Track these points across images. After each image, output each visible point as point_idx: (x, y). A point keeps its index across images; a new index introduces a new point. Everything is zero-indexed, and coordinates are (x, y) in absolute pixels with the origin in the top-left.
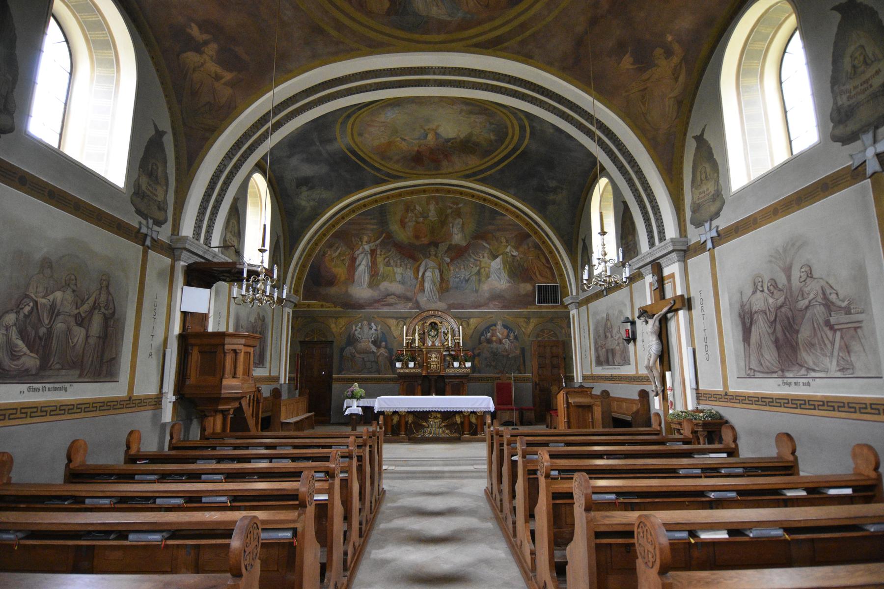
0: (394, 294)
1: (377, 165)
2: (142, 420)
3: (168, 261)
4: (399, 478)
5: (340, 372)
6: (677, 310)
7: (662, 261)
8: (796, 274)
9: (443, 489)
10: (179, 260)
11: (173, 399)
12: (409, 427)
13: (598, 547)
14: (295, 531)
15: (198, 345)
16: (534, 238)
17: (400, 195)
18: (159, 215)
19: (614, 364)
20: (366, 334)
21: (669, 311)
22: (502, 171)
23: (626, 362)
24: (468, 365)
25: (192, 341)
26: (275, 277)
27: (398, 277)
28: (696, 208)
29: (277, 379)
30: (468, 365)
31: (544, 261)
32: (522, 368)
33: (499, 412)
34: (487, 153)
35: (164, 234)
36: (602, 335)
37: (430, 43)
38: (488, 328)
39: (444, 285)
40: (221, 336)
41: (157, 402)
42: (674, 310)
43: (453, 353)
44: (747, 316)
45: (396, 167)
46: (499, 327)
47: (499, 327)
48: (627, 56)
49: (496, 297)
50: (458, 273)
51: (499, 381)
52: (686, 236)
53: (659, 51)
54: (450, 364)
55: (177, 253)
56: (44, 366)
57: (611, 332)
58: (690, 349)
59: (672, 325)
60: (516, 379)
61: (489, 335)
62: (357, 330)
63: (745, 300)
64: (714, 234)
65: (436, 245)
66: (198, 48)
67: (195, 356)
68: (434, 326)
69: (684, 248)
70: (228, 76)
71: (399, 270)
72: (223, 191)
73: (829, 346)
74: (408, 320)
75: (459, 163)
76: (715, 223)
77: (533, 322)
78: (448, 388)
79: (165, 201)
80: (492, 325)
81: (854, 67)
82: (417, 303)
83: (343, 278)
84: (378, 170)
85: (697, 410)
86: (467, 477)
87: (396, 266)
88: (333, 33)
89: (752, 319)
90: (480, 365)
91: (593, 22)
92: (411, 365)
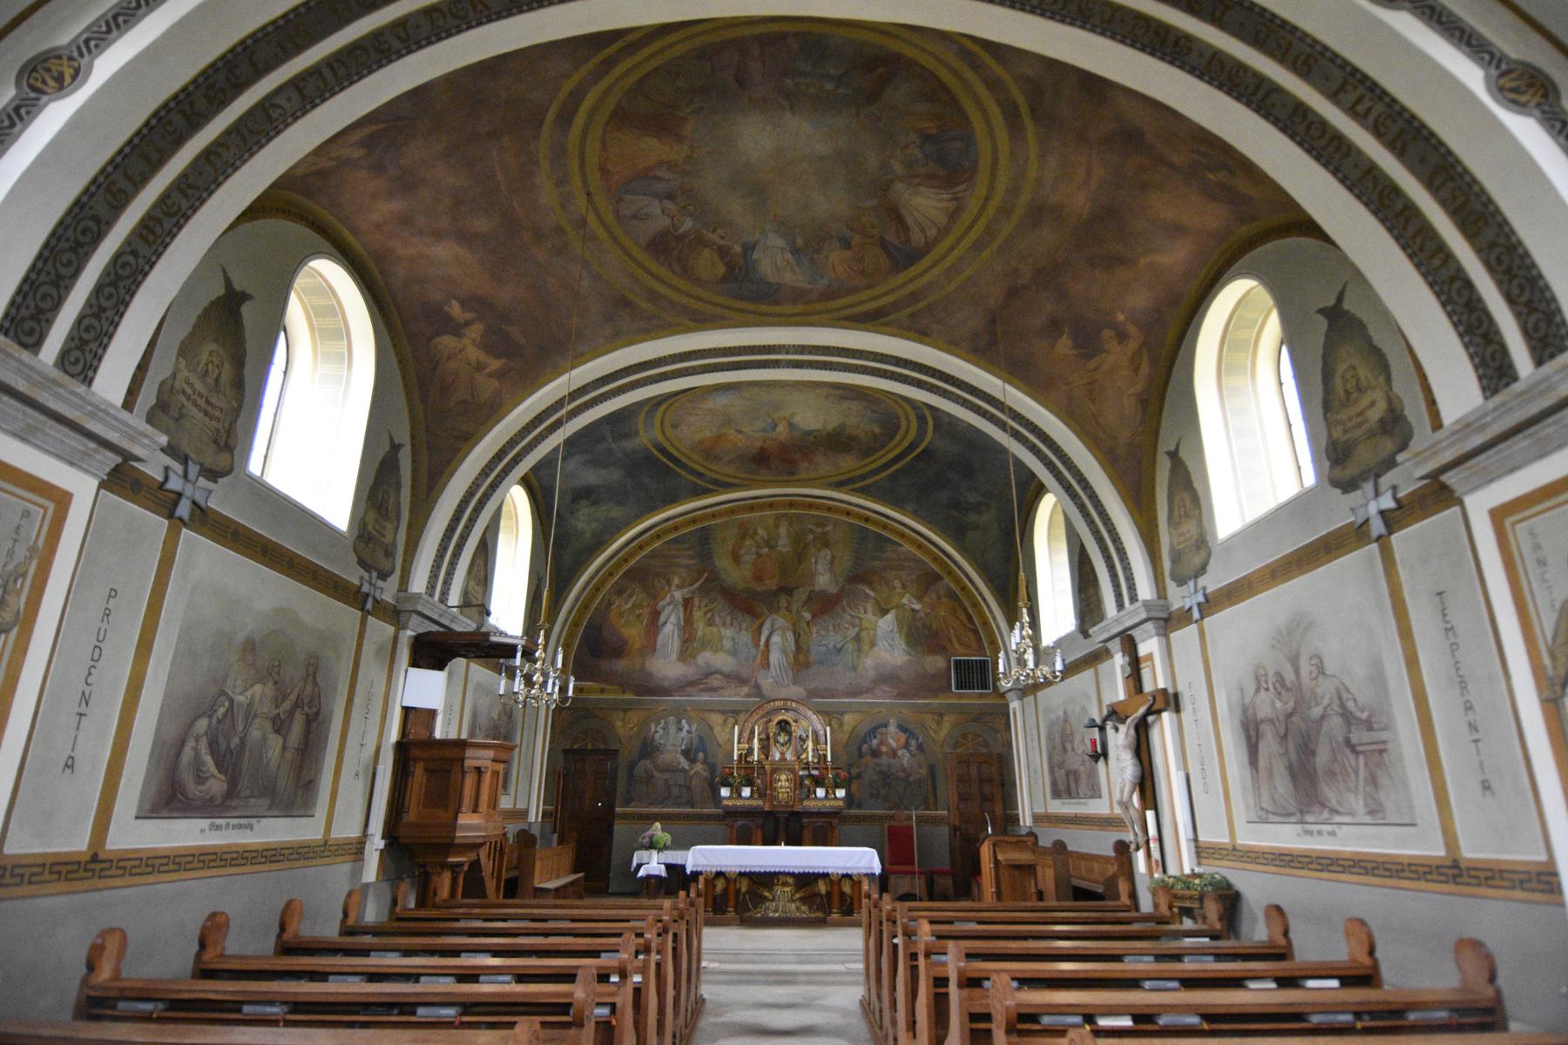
0: (718, 672)
1: (697, 468)
2: (337, 877)
3: (390, 629)
4: (726, 983)
5: (627, 803)
6: (1159, 712)
7: (1135, 633)
8: (1305, 668)
9: (792, 1000)
10: (405, 627)
11: (381, 844)
12: (742, 900)
13: (972, 1030)
14: (613, 1006)
15: (425, 761)
16: (947, 580)
17: (733, 511)
18: (385, 564)
19: (1078, 797)
20: (673, 738)
21: (1149, 712)
22: (893, 477)
23: (1095, 793)
24: (841, 793)
25: (415, 753)
26: (559, 665)
27: (728, 644)
28: (1177, 558)
29: (524, 814)
30: (841, 793)
31: (963, 618)
32: (931, 800)
33: (893, 878)
34: (868, 451)
35: (388, 591)
36: (1059, 747)
37: (780, 315)
38: (873, 732)
39: (801, 657)
40: (460, 745)
41: (356, 850)
42: (1154, 711)
43: (815, 772)
44: (1252, 726)
45: (729, 470)
46: (892, 729)
47: (892, 729)
48: (1065, 337)
49: (887, 678)
50: (824, 638)
51: (893, 823)
52: (1165, 598)
53: (1107, 333)
54: (810, 793)
55: (403, 618)
56: (231, 793)
57: (1072, 742)
58: (1182, 775)
59: (1155, 734)
60: (920, 820)
61: (875, 742)
62: (657, 732)
63: (1247, 701)
64: (1201, 598)
65: (788, 591)
66: (457, 329)
67: (419, 774)
68: (784, 726)
69: (1164, 615)
70: (495, 364)
71: (728, 632)
72: (472, 521)
73: (1353, 776)
74: (742, 717)
75: (824, 465)
76: (1202, 581)
77: (948, 721)
78: (807, 834)
79: (394, 544)
80: (875, 729)
81: (1347, 393)
82: (757, 686)
83: (638, 645)
84: (700, 475)
85: (1194, 875)
86: (833, 983)
87: (724, 625)
88: (645, 305)
89: (1257, 730)
90: (866, 795)
91: (1013, 292)
92: (746, 792)
